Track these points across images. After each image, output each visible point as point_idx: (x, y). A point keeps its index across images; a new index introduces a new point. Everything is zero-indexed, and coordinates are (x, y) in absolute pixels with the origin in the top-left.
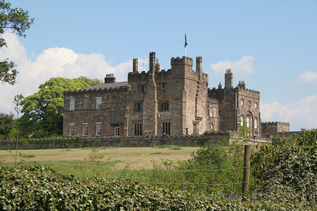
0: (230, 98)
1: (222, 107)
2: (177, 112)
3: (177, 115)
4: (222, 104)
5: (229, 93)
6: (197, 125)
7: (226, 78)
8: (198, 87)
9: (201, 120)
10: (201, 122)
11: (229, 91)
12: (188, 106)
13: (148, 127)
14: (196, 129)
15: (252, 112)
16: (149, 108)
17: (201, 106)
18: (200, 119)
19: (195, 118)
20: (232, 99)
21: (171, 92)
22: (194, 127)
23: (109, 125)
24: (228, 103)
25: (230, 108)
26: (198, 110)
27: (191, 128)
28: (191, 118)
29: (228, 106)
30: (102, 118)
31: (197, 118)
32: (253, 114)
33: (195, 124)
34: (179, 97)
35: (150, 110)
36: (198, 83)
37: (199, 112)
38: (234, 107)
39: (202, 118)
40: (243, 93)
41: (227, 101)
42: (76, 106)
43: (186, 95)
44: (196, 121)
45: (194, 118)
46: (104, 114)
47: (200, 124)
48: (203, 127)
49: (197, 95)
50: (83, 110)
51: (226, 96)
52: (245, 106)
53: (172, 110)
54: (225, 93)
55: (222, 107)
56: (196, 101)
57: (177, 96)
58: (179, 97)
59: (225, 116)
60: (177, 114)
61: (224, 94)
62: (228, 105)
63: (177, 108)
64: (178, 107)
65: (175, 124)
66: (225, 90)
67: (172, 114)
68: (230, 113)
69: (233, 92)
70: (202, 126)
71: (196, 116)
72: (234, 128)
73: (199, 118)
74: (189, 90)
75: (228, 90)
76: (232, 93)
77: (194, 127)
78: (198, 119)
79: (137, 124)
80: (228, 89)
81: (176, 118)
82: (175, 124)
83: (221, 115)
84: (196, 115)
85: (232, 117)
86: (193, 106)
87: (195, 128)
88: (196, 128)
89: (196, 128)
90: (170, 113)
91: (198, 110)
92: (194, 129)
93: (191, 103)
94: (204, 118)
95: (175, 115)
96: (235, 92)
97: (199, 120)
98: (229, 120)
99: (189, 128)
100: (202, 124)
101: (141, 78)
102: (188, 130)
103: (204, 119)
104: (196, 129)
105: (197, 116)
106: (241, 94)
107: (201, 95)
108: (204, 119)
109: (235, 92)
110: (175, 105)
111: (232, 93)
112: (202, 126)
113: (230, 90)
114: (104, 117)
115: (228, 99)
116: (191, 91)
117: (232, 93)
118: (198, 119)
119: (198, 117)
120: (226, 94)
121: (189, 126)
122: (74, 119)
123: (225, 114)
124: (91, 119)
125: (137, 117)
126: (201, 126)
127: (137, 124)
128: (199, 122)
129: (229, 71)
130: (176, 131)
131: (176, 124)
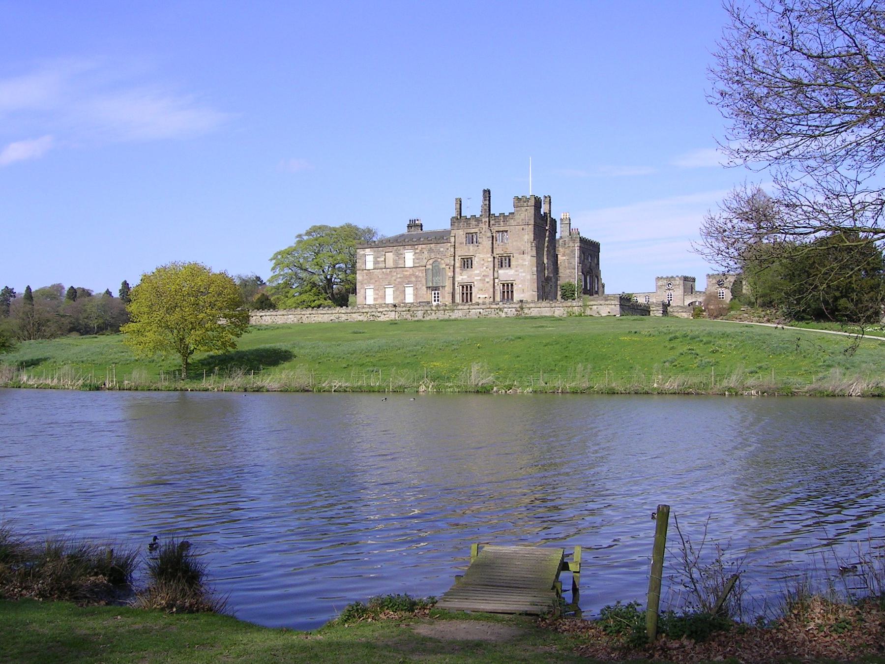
0: (567, 251)
23: (424, 288)
30: (414, 279)
41: (564, 255)
42: (376, 262)
50: (385, 268)
68: (568, 271)
114: (417, 277)
122: (373, 281)
124: (399, 280)
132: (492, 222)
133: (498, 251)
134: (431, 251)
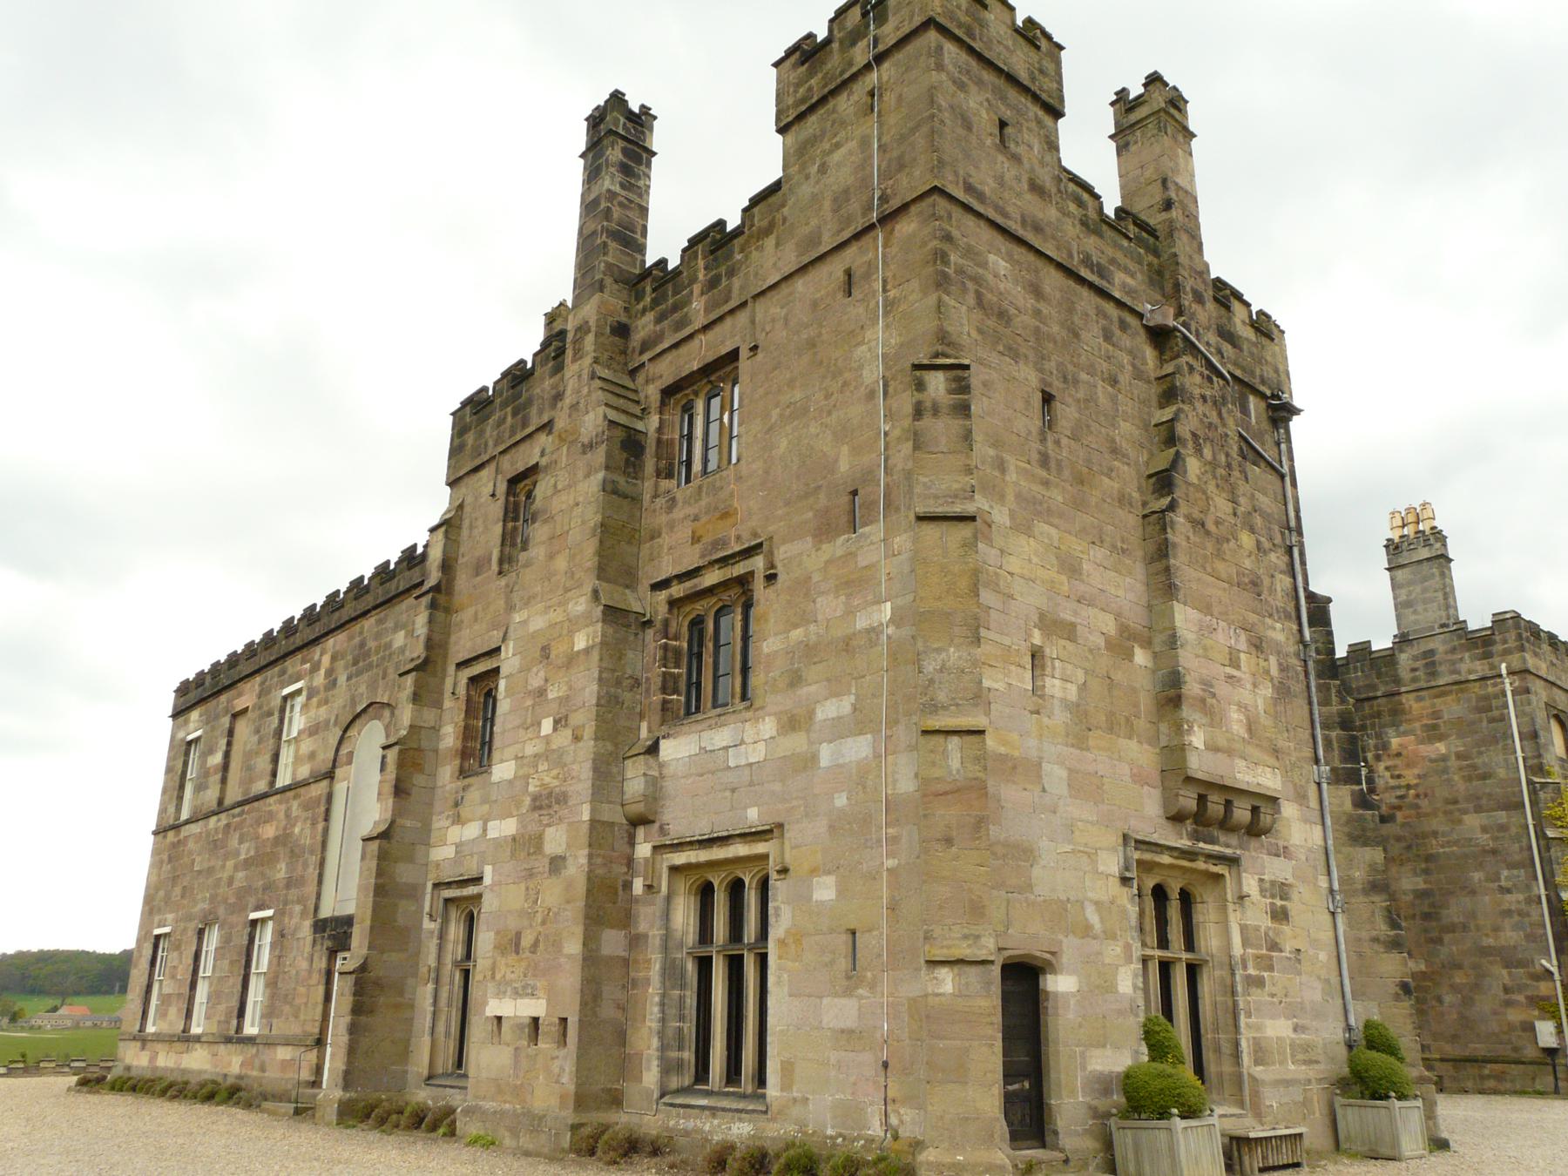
0: (1452, 708)
1: (1393, 782)
3: (858, 748)
4: (1398, 762)
5: (1442, 669)
6: (1205, 915)
7: (1399, 573)
8: (1170, 394)
9: (1255, 830)
10: (1258, 871)
11: (1437, 658)
12: (1030, 600)
13: (516, 946)
14: (1193, 971)
16: (541, 692)
17: (1227, 637)
18: (1242, 814)
19: (1168, 798)
20: (1480, 710)
22: (1163, 943)
24: (1441, 747)
25: (1469, 779)
27: (1113, 951)
28: (1084, 786)
31: (1189, 802)
33: (1170, 905)
34: (869, 476)
35: (547, 726)
36: (1159, 336)
38: (1502, 773)
39: (1274, 800)
40: (1553, 664)
43: (963, 410)
46: (297, 830)
48: (1290, 938)
49: (1164, 481)
50: (221, 808)
55: (1393, 782)
56: (1161, 552)
57: (844, 466)
58: (869, 476)
59: (1435, 846)
60: (860, 722)
61: (1397, 681)
62: (1444, 758)
64: (862, 623)
66: (1403, 658)
67: (796, 743)
68: (1472, 821)
70: (1280, 915)
71: (1173, 768)
72: (1530, 938)
74: (1029, 377)
75: (1432, 652)
76: (1471, 667)
77: (1163, 943)
78: (1219, 817)
80: (1431, 646)
81: (841, 801)
82: (825, 890)
83: (1399, 839)
84: (1174, 755)
85: (1494, 852)
86: (1109, 625)
87: (1177, 951)
88: (1190, 945)
89: (1190, 945)
90: (768, 727)
91: (1207, 684)
92: (1165, 968)
93: (1071, 568)
94: (1289, 810)
95: (826, 754)
98: (1477, 876)
99: (1070, 949)
100: (1281, 890)
101: (529, 402)
102: (1060, 984)
103: (1300, 829)
104: (1193, 971)
105: (1200, 763)
107: (1221, 505)
108: (1300, 829)
109: (1487, 656)
111: (1464, 667)
112: (1280, 915)
115: (1436, 715)
116: (1067, 413)
117: (1464, 667)
119: (1206, 788)
120: (1414, 680)
121: (1061, 913)
123: (1435, 834)
125: (471, 831)
126: (1265, 922)
128: (1233, 861)
131: (842, 891)
132: (644, 326)
133: (673, 551)
134: (360, 659)
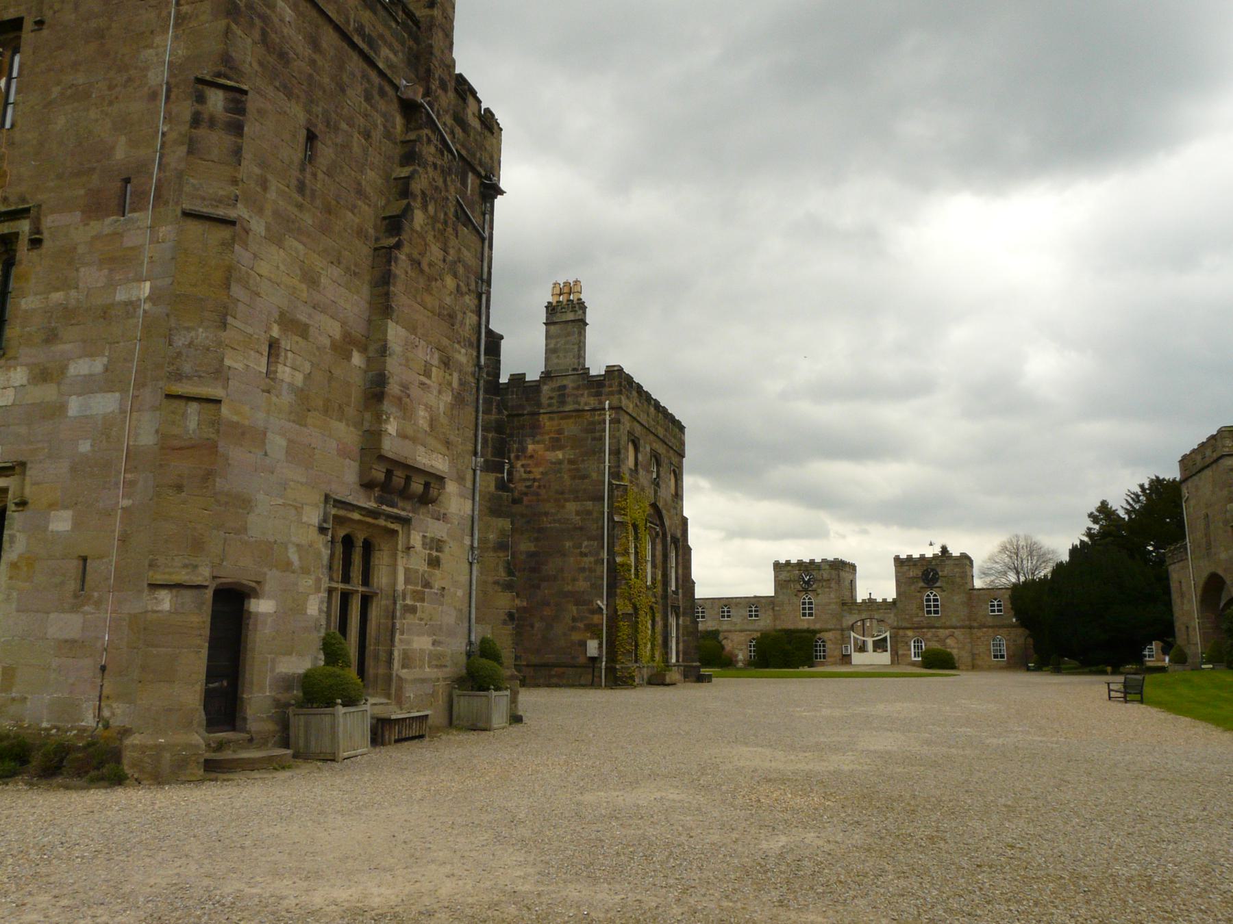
0: (571, 428)
1: (525, 476)
2: (98, 365)
3: (106, 404)
5: (569, 399)
6: (381, 560)
7: (552, 328)
9: (425, 499)
10: (425, 528)
12: (273, 300)
14: (366, 600)
15: (664, 512)
18: (417, 487)
21: (60, 122)
22: (346, 579)
24: (560, 455)
26: (393, 388)
27: (307, 582)
29: (559, 471)
31: (379, 474)
32: (667, 523)
33: (354, 549)
37: (406, 411)
39: (441, 479)
43: (237, 129)
44: (371, 505)
45: (350, 473)
47: (416, 539)
51: (551, 419)
52: (644, 478)
53: (51, 337)
54: (544, 401)
56: (383, 281)
57: (120, 154)
60: (109, 381)
61: (539, 405)
62: (560, 462)
63: (105, 313)
64: (121, 296)
65: (61, 522)
66: (545, 388)
67: (48, 393)
68: (571, 507)
69: (590, 395)
70: (434, 563)
72: (593, 586)
73: (411, 470)
75: (564, 387)
76: (587, 400)
77: (346, 579)
78: (399, 487)
79: (359, 544)
80: (565, 382)
81: (85, 447)
83: (522, 516)
84: (373, 437)
85: (581, 529)
86: (335, 330)
87: (357, 586)
88: (366, 581)
89: (366, 581)
91: (405, 387)
92: (346, 597)
94: (451, 487)
95: (74, 406)
96: (598, 394)
97: (404, 494)
100: (438, 544)
103: (457, 502)
105: (390, 446)
106: (630, 411)
109: (598, 394)
110: (91, 277)
111: (583, 400)
112: (434, 563)
113: (571, 385)
115: (560, 432)
116: (326, 152)
117: (583, 400)
118: (399, 487)
120: (550, 405)
123: (546, 514)
126: (423, 567)
127: (359, 544)
128: (406, 522)
129: (570, 288)
130: (66, 625)
131: (76, 525)
